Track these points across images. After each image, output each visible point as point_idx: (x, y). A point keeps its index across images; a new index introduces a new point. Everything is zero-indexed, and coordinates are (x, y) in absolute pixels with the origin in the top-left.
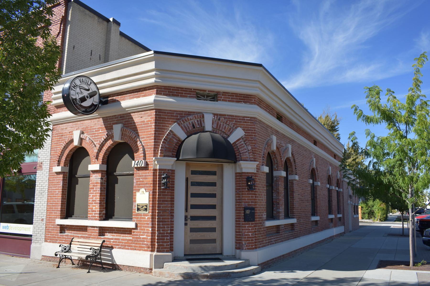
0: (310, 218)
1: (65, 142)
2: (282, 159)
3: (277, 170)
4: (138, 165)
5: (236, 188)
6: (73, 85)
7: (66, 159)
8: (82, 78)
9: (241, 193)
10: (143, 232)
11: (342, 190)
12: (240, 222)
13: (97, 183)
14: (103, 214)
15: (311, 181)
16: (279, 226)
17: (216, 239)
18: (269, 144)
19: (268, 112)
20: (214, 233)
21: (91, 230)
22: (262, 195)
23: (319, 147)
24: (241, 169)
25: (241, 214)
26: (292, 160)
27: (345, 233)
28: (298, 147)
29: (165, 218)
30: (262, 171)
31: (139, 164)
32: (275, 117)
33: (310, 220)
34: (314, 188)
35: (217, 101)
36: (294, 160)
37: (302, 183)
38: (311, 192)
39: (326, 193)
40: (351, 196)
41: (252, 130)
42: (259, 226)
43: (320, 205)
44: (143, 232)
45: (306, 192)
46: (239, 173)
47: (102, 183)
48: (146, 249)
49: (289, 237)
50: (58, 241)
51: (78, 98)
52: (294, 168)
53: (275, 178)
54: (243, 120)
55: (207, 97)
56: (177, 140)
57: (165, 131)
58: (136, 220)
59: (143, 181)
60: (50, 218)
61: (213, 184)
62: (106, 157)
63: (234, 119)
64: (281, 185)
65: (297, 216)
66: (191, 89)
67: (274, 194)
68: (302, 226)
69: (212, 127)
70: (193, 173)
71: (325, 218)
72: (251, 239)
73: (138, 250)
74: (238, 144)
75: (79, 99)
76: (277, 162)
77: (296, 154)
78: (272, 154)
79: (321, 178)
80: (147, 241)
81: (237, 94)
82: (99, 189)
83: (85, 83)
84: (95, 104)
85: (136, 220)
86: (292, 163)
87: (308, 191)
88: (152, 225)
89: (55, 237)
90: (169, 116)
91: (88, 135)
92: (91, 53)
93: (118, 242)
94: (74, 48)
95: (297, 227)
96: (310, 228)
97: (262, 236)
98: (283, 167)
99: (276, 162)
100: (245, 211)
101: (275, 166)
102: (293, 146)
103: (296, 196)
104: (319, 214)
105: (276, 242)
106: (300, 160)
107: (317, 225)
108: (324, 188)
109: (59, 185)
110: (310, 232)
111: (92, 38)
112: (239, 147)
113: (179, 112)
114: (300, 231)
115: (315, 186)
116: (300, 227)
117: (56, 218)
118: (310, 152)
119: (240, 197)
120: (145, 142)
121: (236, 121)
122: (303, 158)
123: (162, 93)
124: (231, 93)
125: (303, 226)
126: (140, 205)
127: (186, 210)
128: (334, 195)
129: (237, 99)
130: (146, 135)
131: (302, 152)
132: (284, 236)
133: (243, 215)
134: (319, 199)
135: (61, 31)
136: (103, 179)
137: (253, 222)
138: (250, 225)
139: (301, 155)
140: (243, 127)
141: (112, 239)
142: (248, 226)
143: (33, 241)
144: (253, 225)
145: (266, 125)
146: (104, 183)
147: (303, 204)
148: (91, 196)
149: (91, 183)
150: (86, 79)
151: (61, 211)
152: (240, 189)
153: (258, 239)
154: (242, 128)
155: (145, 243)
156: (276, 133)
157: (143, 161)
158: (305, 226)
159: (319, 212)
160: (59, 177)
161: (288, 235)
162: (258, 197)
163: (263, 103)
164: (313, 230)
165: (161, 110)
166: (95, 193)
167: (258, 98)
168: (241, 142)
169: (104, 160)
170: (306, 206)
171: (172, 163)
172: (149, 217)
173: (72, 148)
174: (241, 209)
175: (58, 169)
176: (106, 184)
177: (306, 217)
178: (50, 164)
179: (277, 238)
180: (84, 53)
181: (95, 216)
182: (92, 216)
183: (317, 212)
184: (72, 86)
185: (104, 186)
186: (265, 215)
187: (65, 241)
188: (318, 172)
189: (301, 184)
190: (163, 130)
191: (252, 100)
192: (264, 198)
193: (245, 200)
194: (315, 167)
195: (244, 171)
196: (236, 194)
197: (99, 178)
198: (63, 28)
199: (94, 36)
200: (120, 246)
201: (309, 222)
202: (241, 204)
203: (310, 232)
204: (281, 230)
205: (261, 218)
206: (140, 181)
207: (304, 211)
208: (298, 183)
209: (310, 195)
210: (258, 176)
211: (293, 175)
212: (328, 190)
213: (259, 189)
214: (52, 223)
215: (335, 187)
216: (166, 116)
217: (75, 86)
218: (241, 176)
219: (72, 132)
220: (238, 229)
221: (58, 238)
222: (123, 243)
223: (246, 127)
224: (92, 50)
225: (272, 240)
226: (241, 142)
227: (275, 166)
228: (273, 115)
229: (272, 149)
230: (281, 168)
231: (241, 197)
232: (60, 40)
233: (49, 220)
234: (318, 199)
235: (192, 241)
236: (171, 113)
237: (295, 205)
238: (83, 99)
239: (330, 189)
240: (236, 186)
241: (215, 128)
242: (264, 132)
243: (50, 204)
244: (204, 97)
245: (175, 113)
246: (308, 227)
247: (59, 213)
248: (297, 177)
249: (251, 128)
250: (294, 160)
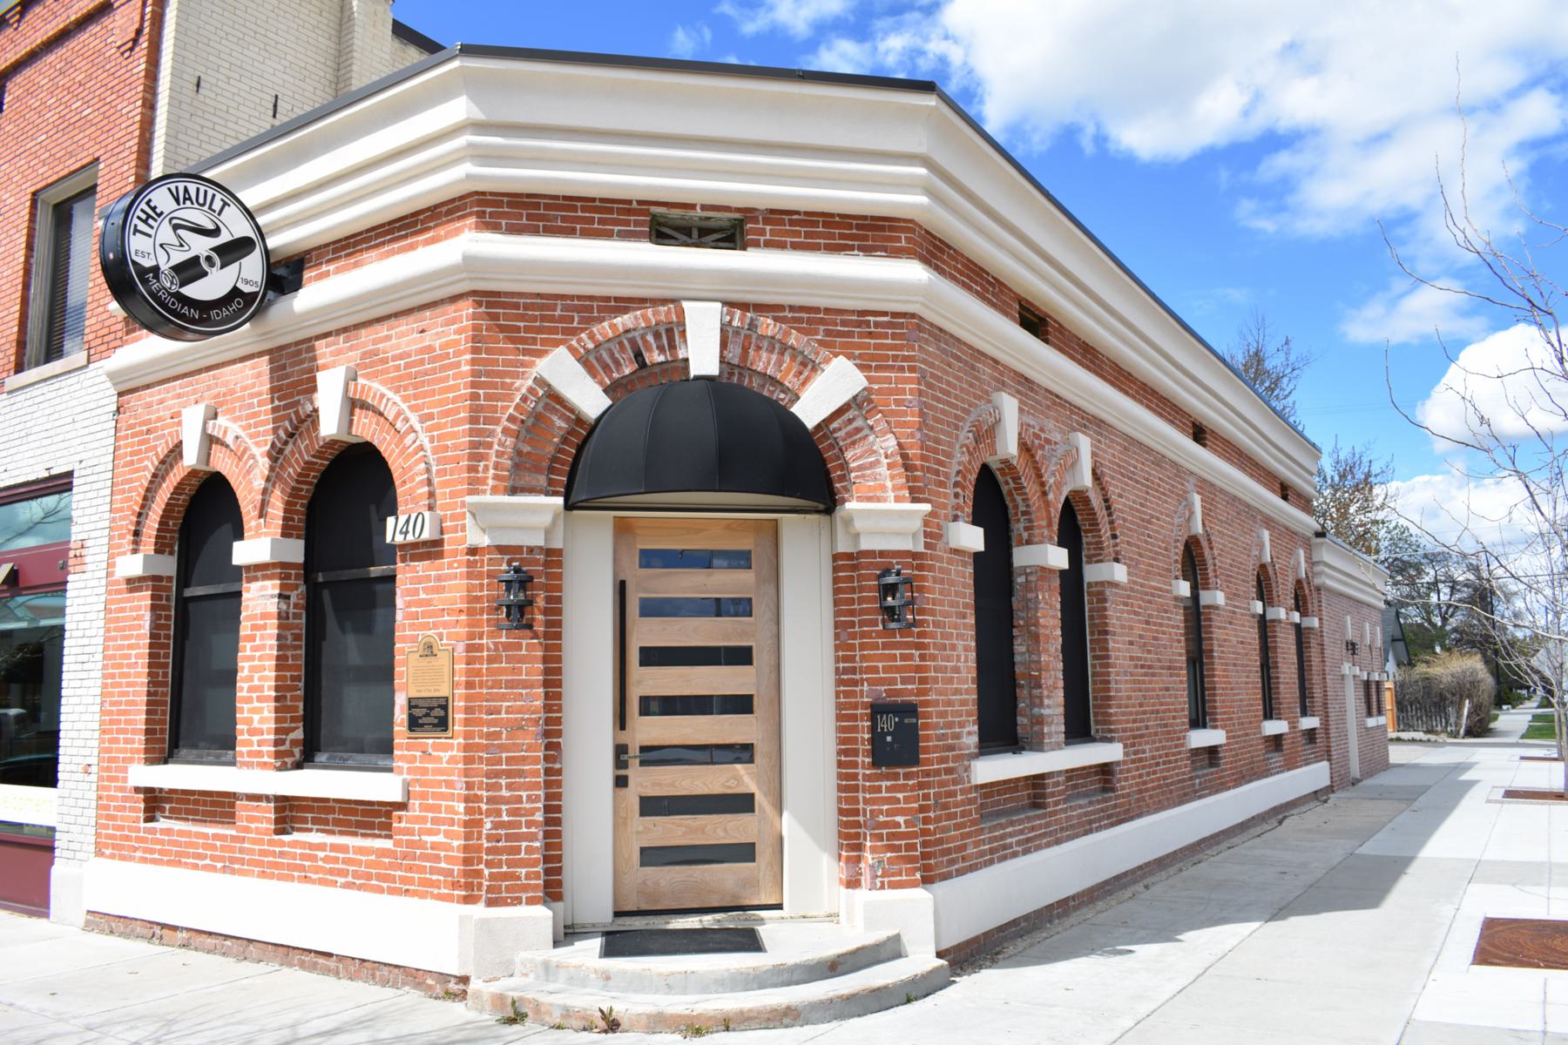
0: (1184, 737)
1: (157, 455)
2: (1051, 496)
3: (1029, 542)
4: (407, 533)
5: (836, 622)
6: (142, 211)
7: (161, 523)
8: (181, 186)
9: (857, 642)
10: (435, 821)
11: (1315, 623)
12: (857, 767)
13: (264, 616)
14: (294, 743)
15: (1184, 588)
16: (1042, 776)
17: (753, 844)
18: (986, 433)
19: (977, 293)
20: (744, 818)
21: (246, 808)
22: (953, 647)
23: (1215, 451)
24: (856, 537)
25: (859, 735)
26: (1096, 501)
27: (1333, 792)
28: (1125, 448)
29: (524, 760)
30: (953, 545)
31: (411, 529)
32: (1013, 318)
33: (1182, 745)
34: (1196, 617)
35: (744, 248)
36: (1106, 501)
37: (1147, 594)
38: (1186, 634)
39: (1253, 635)
40: (1353, 644)
42: (942, 784)
43: (1225, 683)
44: (435, 821)
45: (1164, 633)
46: (849, 556)
47: (284, 615)
48: (446, 891)
49: (1090, 822)
50: (139, 854)
51: (164, 267)
52: (1109, 534)
53: (1020, 575)
54: (859, 324)
55: (700, 237)
56: (567, 420)
57: (516, 385)
58: (409, 768)
59: (428, 602)
60: (110, 760)
61: (741, 607)
62: (298, 507)
63: (822, 322)
64: (1046, 603)
65: (1124, 730)
66: (629, 202)
68: (1148, 774)
69: (722, 357)
70: (650, 559)
71: (1247, 735)
72: (903, 842)
73: (415, 894)
74: (840, 429)
76: (1028, 506)
77: (1113, 478)
78: (1003, 474)
79: (1228, 576)
80: (448, 859)
81: (832, 215)
82: (275, 642)
83: (196, 206)
84: (247, 289)
85: (406, 766)
86: (1095, 514)
87: (1173, 627)
88: (467, 789)
89: (127, 838)
90: (534, 319)
91: (235, 420)
92: (275, 106)
94: (198, 85)
95: (1126, 779)
96: (1184, 780)
97: (958, 827)
98: (1056, 527)
99: (1022, 508)
100: (873, 718)
101: (1021, 526)
102: (1099, 441)
103: (1119, 650)
104: (1222, 720)
105: (1028, 847)
106: (1134, 502)
107: (1218, 765)
108: (1242, 614)
109: (140, 627)
110: (1185, 795)
111: (279, 46)
112: (841, 443)
113: (576, 302)
114: (1140, 792)
115: (1205, 607)
116: (1140, 776)
117: (131, 760)
118: (1179, 471)
119: (852, 659)
120: (435, 433)
121: (828, 333)
122: (1147, 493)
123: (504, 222)
124: (806, 213)
125: (1155, 773)
126: (421, 703)
127: (621, 721)
128: (1286, 646)
129: (832, 236)
130: (441, 403)
131: (1142, 470)
132: (1069, 818)
133: (867, 736)
134: (1220, 658)
135: (147, 24)
136: (288, 597)
137: (915, 769)
138: (901, 782)
139: (1137, 482)
140: (860, 357)
141: (322, 847)
142: (889, 783)
143: (57, 853)
144: (911, 782)
145: (970, 347)
146: (296, 616)
147: (1150, 683)
149: (249, 618)
150: (202, 189)
151: (147, 732)
152: (852, 625)
153: (940, 841)
154: (858, 362)
155: (443, 865)
156: (1019, 383)
157: (427, 514)
158: (1162, 771)
159: (1224, 713)
160: (140, 599)
161: (1086, 814)
162: (933, 658)
163: (949, 255)
164: (1197, 787)
165: (498, 294)
166: (261, 658)
167: (927, 232)
168: (850, 421)
169: (293, 520)
170: (1167, 689)
171: (547, 519)
172: (455, 753)
173: (183, 479)
174: (859, 711)
175: (133, 565)
176: (304, 621)
177: (1169, 733)
178: (111, 547)
179: (1033, 829)
180: (241, 108)
181: (260, 752)
182: (250, 754)
183: (1216, 714)
184: (139, 218)
185: (297, 626)
186: (969, 733)
187: (161, 852)
188: (1216, 552)
189: (1143, 600)
190: (508, 380)
191: (899, 239)
192: (966, 661)
193: (875, 670)
194: (1200, 530)
195: (865, 545)
196: (837, 648)
197: (272, 596)
198: (153, 11)
199: (283, 41)
200: (350, 879)
201: (1180, 753)
202: (858, 689)
203: (1185, 795)
204: (1053, 795)
205: (951, 748)
206: (420, 603)
207: (1158, 712)
208: (1129, 597)
209: (1183, 644)
210: (931, 568)
211: (1101, 561)
212: (1259, 622)
213: (937, 624)
214: (115, 779)
215: (1289, 610)
216: (522, 318)
217: (149, 216)
218: (854, 568)
219: (179, 414)
220: (848, 801)
221: (138, 839)
222: (359, 863)
223: (873, 358)
224: (276, 97)
225: (1009, 840)
227: (1018, 527)
228: (1003, 309)
229: (1001, 455)
230: (1046, 532)
231: (857, 658)
232: (143, 60)
233: (108, 769)
234: (1216, 661)
235: (652, 856)
236: (542, 307)
237: (1113, 685)
238: (190, 270)
239: (1269, 617)
240: (837, 614)
241: (736, 361)
242: (959, 379)
243: (112, 704)
244: (690, 237)
245: (559, 307)
246: (1177, 775)
247: (139, 741)
248: (1120, 573)
249: (895, 358)
250: (1106, 501)
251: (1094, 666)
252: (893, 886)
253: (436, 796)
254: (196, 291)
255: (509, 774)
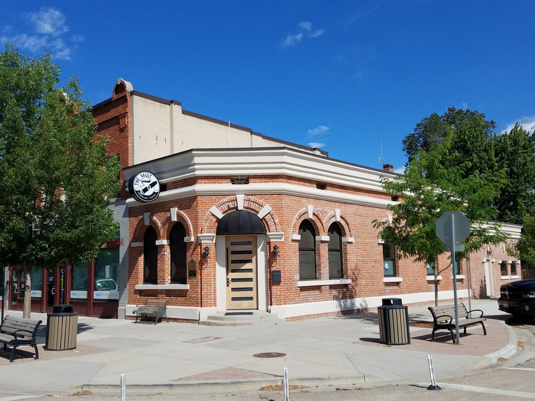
41: (280, 205)
51: (141, 190)
63: (264, 197)
66: (226, 176)
67: (316, 257)
75: (142, 190)
90: (209, 200)
93: (178, 301)
121: (265, 199)
124: (261, 175)
148: (159, 266)
150: (146, 173)
168: (269, 217)
216: (207, 200)
226: (269, 217)
238: (145, 190)
248: (350, 239)
249: (278, 203)
251: (344, 262)
252: (277, 305)
253: (194, 288)
254: (147, 194)
255: (206, 283)
